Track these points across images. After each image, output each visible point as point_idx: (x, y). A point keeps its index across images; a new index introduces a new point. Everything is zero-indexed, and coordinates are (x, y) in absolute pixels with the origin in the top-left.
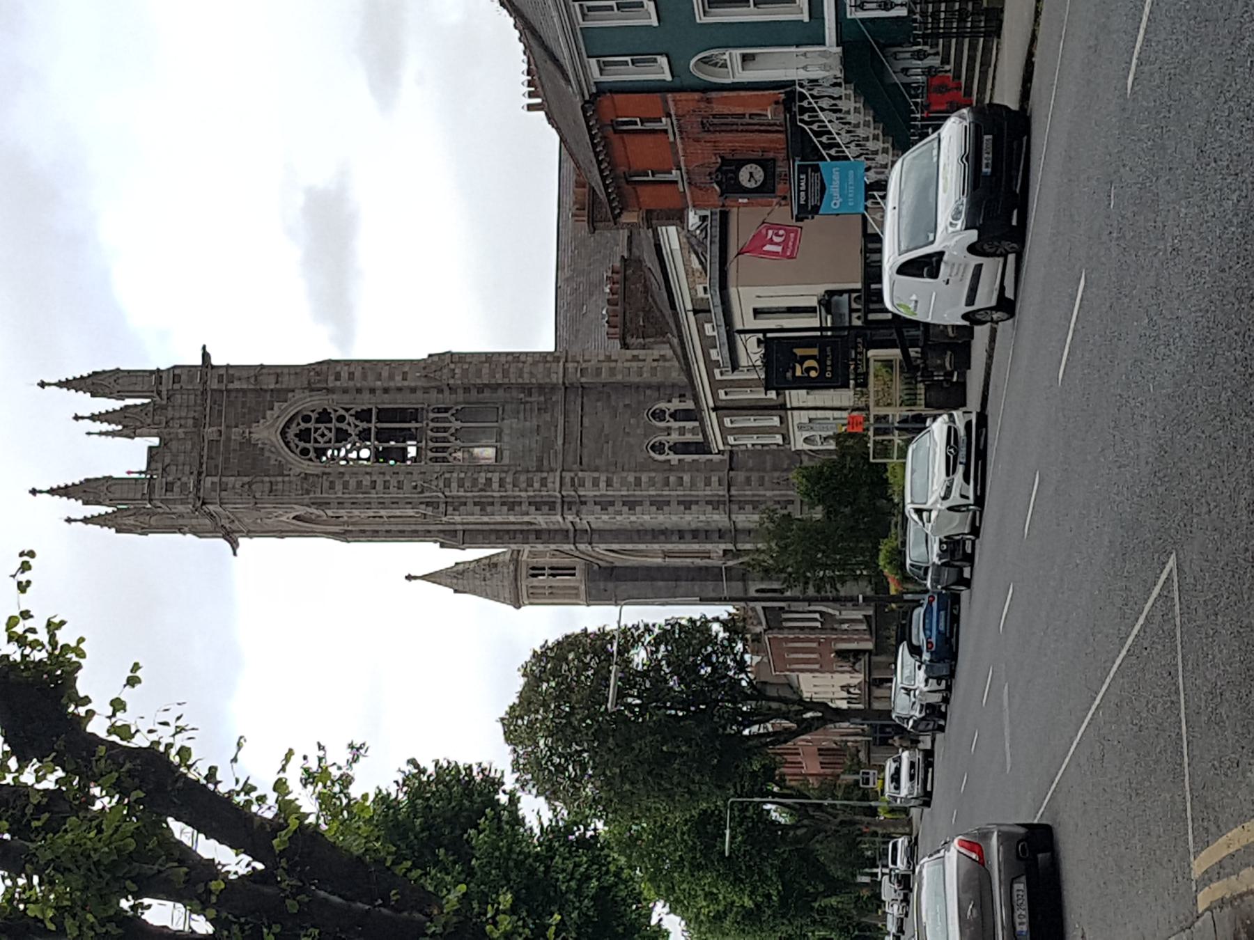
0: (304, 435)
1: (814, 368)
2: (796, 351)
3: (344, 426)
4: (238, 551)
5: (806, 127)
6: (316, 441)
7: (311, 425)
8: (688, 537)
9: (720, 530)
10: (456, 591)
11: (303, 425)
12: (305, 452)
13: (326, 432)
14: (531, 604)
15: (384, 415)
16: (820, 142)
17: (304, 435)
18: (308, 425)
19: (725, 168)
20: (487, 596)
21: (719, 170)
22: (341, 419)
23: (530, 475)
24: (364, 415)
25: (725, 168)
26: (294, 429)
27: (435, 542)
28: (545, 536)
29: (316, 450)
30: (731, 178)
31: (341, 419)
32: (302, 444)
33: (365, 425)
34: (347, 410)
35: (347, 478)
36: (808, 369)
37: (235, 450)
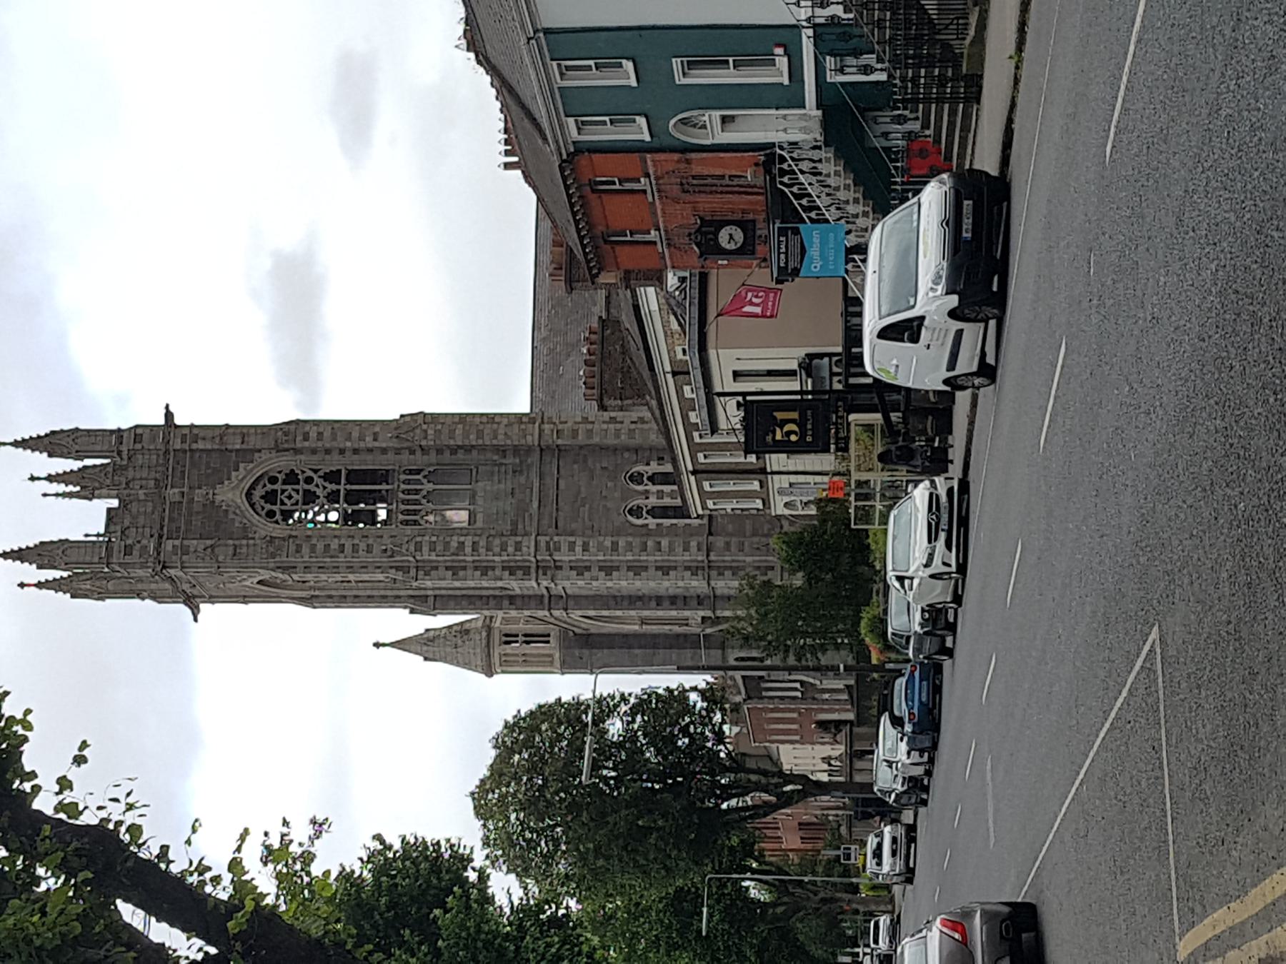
0: (270, 497)
1: (794, 432)
2: (775, 414)
3: (312, 487)
4: (200, 617)
5: (786, 190)
6: (283, 503)
7: (278, 487)
8: (666, 603)
9: (699, 597)
10: (426, 659)
11: (269, 487)
12: (271, 514)
13: (293, 494)
14: (503, 672)
15: (354, 476)
16: (791, 192)
17: (270, 497)
18: (275, 487)
19: (704, 229)
20: (458, 664)
21: (698, 231)
22: (309, 480)
23: (504, 539)
24: (332, 477)
25: (704, 229)
26: (258, 492)
27: (405, 607)
28: (519, 602)
29: (283, 512)
30: (711, 239)
31: (309, 480)
32: (268, 507)
33: (334, 487)
34: (316, 471)
35: (314, 541)
36: (789, 433)
37: (198, 513)
